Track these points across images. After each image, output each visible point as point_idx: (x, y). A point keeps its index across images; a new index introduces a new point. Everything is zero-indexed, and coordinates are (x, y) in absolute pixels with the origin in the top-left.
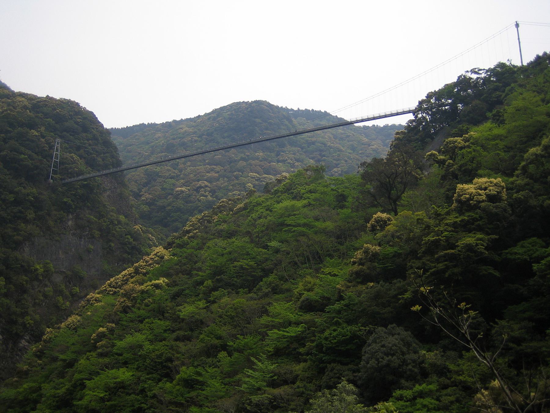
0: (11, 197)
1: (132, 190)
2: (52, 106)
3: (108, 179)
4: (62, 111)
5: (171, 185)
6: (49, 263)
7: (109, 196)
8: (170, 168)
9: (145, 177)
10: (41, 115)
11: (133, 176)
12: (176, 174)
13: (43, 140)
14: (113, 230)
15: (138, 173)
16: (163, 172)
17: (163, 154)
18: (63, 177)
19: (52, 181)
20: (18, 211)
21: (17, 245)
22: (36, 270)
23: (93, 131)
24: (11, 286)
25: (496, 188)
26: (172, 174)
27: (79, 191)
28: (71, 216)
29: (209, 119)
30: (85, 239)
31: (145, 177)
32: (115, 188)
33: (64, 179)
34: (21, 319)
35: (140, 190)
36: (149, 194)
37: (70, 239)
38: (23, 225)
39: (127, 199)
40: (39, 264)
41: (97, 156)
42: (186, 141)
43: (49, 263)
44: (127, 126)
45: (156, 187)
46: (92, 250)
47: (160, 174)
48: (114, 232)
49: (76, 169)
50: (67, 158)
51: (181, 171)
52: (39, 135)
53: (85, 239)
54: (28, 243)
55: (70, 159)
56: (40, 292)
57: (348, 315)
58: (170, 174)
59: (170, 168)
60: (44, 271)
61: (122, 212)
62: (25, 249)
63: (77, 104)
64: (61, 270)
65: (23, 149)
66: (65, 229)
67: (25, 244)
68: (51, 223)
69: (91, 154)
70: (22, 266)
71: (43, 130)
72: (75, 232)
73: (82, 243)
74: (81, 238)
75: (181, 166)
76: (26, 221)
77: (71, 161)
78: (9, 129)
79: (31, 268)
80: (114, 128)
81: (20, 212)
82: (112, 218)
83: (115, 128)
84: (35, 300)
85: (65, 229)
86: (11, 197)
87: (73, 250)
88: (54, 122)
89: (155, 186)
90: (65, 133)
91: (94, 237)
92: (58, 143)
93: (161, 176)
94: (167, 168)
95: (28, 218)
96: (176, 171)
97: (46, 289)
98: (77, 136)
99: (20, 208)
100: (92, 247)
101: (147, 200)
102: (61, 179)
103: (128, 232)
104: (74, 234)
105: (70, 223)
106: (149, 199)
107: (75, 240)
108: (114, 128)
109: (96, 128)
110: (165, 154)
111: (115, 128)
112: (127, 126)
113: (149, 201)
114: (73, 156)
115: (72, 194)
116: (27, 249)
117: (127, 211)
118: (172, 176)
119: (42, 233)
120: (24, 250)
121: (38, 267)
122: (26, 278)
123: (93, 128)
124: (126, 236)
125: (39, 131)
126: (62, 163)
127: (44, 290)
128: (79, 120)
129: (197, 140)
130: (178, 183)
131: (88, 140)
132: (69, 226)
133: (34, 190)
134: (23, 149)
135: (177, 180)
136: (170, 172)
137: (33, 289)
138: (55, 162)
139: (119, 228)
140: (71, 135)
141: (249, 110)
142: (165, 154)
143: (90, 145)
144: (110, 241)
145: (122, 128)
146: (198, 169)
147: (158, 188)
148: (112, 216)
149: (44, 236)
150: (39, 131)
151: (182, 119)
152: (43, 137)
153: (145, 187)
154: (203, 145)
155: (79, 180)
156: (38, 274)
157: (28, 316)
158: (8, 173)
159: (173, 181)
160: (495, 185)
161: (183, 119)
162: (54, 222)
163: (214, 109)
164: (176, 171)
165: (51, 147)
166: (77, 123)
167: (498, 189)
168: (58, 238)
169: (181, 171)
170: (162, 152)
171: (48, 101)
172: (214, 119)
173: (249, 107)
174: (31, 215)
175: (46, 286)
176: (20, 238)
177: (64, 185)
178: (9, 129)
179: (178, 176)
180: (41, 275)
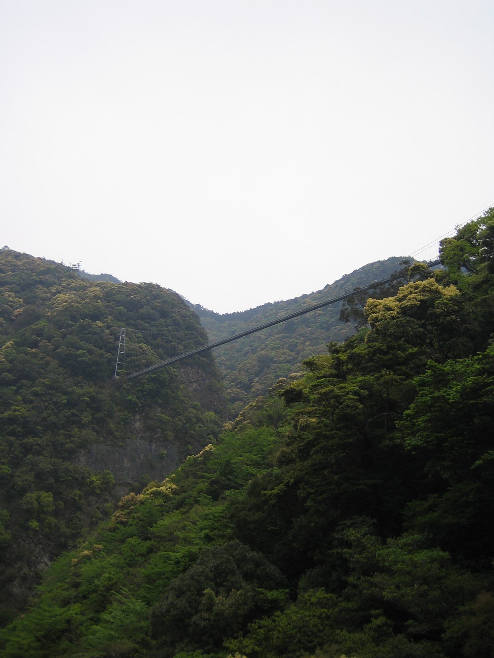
0: (64, 399)
1: (241, 381)
2: (127, 292)
3: (193, 370)
4: (137, 297)
5: (286, 371)
6: (109, 474)
7: (195, 390)
8: (286, 351)
9: (257, 365)
10: (113, 304)
11: (245, 365)
12: (293, 357)
13: (107, 331)
14: (191, 430)
15: (250, 361)
16: (278, 356)
17: (281, 335)
18: (129, 371)
19: (118, 376)
20: (71, 414)
21: (71, 455)
22: (92, 482)
23: (173, 316)
24: (60, 502)
25: (420, 295)
26: (288, 358)
27: (146, 386)
28: (138, 417)
29: (336, 287)
30: (156, 443)
31: (257, 365)
32: (203, 379)
33: (130, 374)
34: (71, 542)
35: (251, 381)
36: (261, 384)
37: (138, 444)
38: (76, 430)
39: (219, 392)
40: (95, 475)
41: (178, 343)
42: (308, 316)
43: (109, 474)
44: (251, 309)
45: (268, 375)
46: (164, 456)
47: (274, 359)
48: (192, 432)
49: (143, 361)
50: (134, 349)
51: (298, 353)
52: (104, 326)
53: (156, 443)
54: (83, 452)
55: (138, 350)
56: (98, 508)
57: (128, 508)
58: (286, 358)
59: (286, 351)
60: (102, 484)
61: (213, 407)
62: (81, 459)
63: (158, 286)
64: (126, 481)
65: (82, 344)
66: (131, 432)
67: (80, 452)
68: (112, 426)
69: (172, 342)
70: (76, 479)
71: (109, 320)
72: (144, 435)
73: (153, 447)
74: (151, 442)
75: (300, 347)
76: (82, 426)
77: (140, 352)
78: (71, 323)
79: (86, 480)
80: (236, 312)
81: (74, 415)
82: (190, 416)
83: (238, 312)
84: (92, 518)
85: (131, 432)
86: (64, 399)
87: (142, 457)
88: (126, 310)
89: (268, 374)
90: (139, 321)
91: (167, 440)
92: (123, 333)
93: (275, 361)
94: (282, 351)
95: (83, 422)
96: (292, 354)
97: (106, 504)
98: (153, 323)
99: (74, 411)
100: (165, 452)
101: (258, 392)
102: (127, 374)
103: (211, 431)
104: (142, 438)
105: (137, 425)
106: (260, 390)
107: (144, 444)
108: (236, 312)
109: (177, 311)
110: (283, 334)
111: (238, 312)
112: (251, 309)
113: (260, 392)
114: (142, 345)
115: (138, 390)
116: (82, 459)
117: (219, 406)
118: (288, 359)
119: (102, 439)
120: (79, 460)
121: (94, 479)
122: (78, 492)
123: (175, 312)
124: (207, 436)
125: (105, 322)
126: (128, 356)
127: (104, 506)
128: (156, 304)
129: (322, 314)
130: (294, 368)
131: (167, 326)
132: (135, 428)
133: (92, 390)
134: (82, 344)
135: (293, 365)
136: (286, 356)
137: (89, 505)
138: (121, 355)
139: (200, 427)
140: (146, 323)
141: (380, 269)
142: (283, 334)
143: (169, 331)
144: (189, 443)
145: (245, 311)
146: (318, 349)
147: (271, 376)
148: (190, 413)
149: (104, 442)
150: (105, 322)
151: (313, 292)
152: (108, 327)
153: (257, 376)
154: (328, 319)
155: (145, 373)
156: (94, 488)
157: (80, 537)
158: (63, 372)
159: (288, 366)
160: (423, 290)
161: (315, 292)
162: (117, 425)
163: (344, 274)
164: (292, 354)
165: (116, 339)
166: (154, 308)
167: (426, 296)
168: (121, 444)
169: (298, 353)
170: (280, 333)
171: (122, 287)
172: (342, 286)
173: (381, 267)
174: (86, 417)
175: (106, 501)
176: (72, 445)
177: (130, 380)
178: (71, 323)
179: (294, 359)
180: (98, 488)
